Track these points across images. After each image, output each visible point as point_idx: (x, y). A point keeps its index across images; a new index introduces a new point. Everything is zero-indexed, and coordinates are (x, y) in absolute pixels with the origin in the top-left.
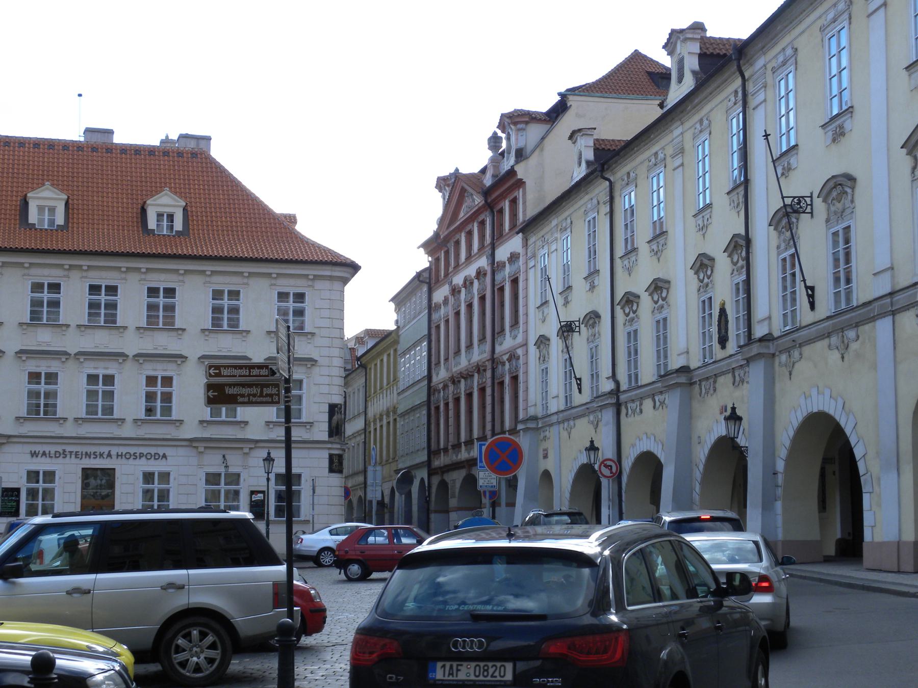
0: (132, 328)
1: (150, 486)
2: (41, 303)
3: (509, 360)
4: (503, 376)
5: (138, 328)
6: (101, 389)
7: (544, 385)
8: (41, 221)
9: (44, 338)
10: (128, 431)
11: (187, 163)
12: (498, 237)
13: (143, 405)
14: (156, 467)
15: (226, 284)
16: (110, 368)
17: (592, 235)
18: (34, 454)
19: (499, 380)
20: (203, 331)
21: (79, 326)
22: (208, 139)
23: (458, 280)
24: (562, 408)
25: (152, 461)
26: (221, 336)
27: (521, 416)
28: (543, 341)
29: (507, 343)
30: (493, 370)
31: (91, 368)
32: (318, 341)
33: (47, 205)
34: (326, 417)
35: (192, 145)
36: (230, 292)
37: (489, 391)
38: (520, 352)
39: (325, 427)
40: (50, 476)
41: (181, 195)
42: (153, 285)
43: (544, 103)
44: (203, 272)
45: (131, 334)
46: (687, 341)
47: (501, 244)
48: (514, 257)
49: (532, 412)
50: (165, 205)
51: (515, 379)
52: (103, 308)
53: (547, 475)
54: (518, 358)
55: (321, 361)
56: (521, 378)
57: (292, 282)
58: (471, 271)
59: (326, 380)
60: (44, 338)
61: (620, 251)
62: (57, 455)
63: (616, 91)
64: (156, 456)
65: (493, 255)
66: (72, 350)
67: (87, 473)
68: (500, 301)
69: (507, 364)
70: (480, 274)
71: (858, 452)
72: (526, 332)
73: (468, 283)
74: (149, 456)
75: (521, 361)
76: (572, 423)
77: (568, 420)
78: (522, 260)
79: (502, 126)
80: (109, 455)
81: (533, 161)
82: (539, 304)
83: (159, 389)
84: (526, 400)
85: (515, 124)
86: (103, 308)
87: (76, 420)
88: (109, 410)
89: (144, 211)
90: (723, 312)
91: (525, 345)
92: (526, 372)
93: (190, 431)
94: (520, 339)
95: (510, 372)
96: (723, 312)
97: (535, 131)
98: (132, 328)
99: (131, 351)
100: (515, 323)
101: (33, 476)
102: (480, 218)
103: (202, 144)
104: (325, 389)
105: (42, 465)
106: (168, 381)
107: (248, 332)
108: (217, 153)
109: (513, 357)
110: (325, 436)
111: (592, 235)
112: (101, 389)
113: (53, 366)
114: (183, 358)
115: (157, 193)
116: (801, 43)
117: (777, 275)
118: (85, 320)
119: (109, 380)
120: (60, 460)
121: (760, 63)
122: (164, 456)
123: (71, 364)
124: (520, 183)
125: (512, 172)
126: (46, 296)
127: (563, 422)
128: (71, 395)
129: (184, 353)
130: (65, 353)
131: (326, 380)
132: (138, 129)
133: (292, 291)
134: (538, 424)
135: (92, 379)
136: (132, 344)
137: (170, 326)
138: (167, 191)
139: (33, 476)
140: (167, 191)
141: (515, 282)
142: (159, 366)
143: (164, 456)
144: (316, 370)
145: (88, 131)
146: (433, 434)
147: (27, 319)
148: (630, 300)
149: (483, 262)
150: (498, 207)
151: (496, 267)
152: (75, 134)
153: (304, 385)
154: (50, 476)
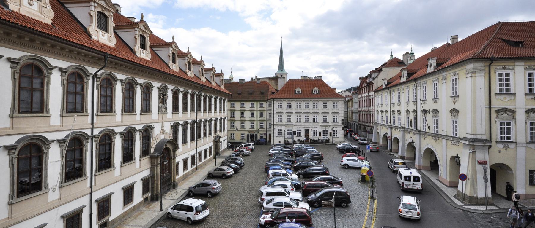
7: (378, 118)
9: (299, 111)
10: (311, 124)
12: (369, 91)
14: (315, 129)
16: (308, 115)
17: (386, 98)
19: (370, 115)
23: (363, 95)
29: (371, 109)
31: (305, 115)
40: (300, 130)
46: (404, 123)
48: (372, 95)
50: (316, 90)
53: (378, 132)
60: (299, 111)
61: (392, 102)
67: (306, 130)
68: (370, 102)
71: (438, 159)
81: (376, 79)
90: (411, 121)
93: (321, 124)
96: (411, 121)
97: (376, 74)
101: (298, 130)
105: (299, 129)
106: (326, 116)
111: (386, 98)
112: (307, 118)
113: (300, 115)
116: (428, 82)
117: (422, 121)
119: (308, 116)
121: (419, 81)
125: (372, 82)
128: (303, 119)
134: (377, 124)
135: (306, 116)
136: (311, 111)
139: (298, 130)
148: (393, 111)
149: (367, 94)
151: (369, 96)
154: (300, 130)
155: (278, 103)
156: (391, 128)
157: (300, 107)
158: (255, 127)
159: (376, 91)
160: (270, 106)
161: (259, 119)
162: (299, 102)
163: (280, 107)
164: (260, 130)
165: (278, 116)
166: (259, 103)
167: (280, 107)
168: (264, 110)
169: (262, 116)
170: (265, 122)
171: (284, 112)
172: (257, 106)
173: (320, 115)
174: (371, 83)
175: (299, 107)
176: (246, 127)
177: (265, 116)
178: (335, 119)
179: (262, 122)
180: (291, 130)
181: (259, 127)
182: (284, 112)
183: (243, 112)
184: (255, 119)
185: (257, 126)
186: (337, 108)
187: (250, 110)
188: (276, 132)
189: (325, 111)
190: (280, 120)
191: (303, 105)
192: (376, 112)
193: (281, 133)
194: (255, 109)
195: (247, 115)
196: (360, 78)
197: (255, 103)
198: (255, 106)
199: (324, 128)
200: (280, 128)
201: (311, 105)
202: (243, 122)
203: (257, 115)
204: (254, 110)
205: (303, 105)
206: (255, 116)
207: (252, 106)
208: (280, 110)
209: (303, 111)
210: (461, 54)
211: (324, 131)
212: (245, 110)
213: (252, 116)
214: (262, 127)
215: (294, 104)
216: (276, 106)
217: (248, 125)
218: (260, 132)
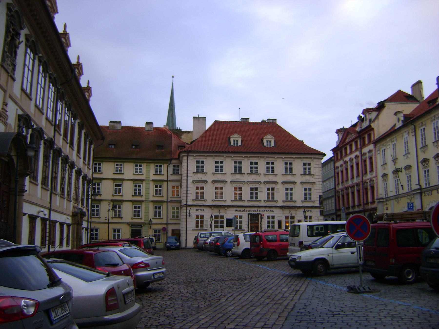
0: (262, 174)
1: (269, 220)
2: (218, 167)
3: (370, 182)
4: (367, 186)
5: (264, 174)
6: (254, 192)
8: (268, 145)
9: (238, 177)
11: (271, 126)
12: (364, 145)
13: (266, 196)
14: (271, 214)
15: (200, 159)
18: (236, 211)
19: (367, 188)
20: (282, 174)
21: (248, 174)
22: (276, 120)
24: (395, 194)
25: (270, 213)
26: (288, 176)
27: (376, 198)
28: (385, 176)
30: (363, 184)
32: (316, 177)
33: (236, 139)
34: (318, 199)
35: (271, 121)
36: (239, 162)
37: (361, 191)
38: (374, 179)
39: (318, 202)
41: (273, 135)
42: (252, 161)
43: (374, 105)
44: (282, 158)
45: (262, 176)
47: (364, 148)
48: (370, 151)
49: (380, 196)
51: (372, 187)
52: (254, 170)
54: (374, 181)
55: (317, 183)
56: (375, 187)
57: (307, 160)
58: (353, 156)
59: (318, 188)
60: (238, 177)
62: (243, 211)
63: (389, 101)
64: (271, 211)
65: (361, 151)
66: (246, 181)
68: (366, 164)
69: (369, 183)
70: (356, 157)
72: (376, 173)
73: (351, 160)
74: (268, 211)
75: (375, 182)
76: (399, 199)
77: (397, 198)
78: (373, 152)
79: (363, 113)
80: (257, 211)
81: (376, 122)
82: (382, 164)
83: (289, 192)
84: (377, 193)
85: (368, 112)
86: (254, 170)
87: (248, 201)
88: (256, 198)
89: (262, 141)
91: (376, 177)
92: (377, 185)
94: (374, 175)
95: (370, 185)
97: (374, 114)
98: (262, 174)
99: (262, 180)
100: (372, 170)
102: (356, 140)
103: (274, 121)
104: (318, 191)
106: (291, 189)
107: (207, 173)
108: (278, 123)
109: (371, 180)
110: (318, 205)
112: (254, 192)
114: (226, 182)
115: (266, 135)
118: (265, 172)
120: (244, 212)
122: (273, 211)
123: (246, 185)
124: (373, 129)
126: (200, 164)
127: (395, 199)
129: (207, 180)
130: (261, 182)
131: (318, 188)
132: (256, 117)
133: (307, 162)
135: (252, 189)
136: (262, 179)
137: (257, 173)
138: (236, 134)
140: (236, 134)
141: (371, 158)
142: (254, 185)
143: (273, 211)
144: (315, 185)
145: (242, 119)
146: (337, 203)
147: (303, 173)
150: (363, 136)
152: (239, 120)
153: (293, 190)
155: (198, 162)
156: (421, 194)
157: (240, 171)
158: (143, 214)
159: (376, 142)
160: (177, 171)
161: (151, 198)
162: (238, 160)
163: (200, 169)
164: (154, 221)
165: (197, 188)
166: (153, 167)
167: (200, 169)
168: (163, 181)
169: (158, 193)
170: (165, 205)
171: (210, 180)
172: (149, 171)
173: (280, 186)
174: (369, 129)
175: (238, 170)
176: (123, 214)
177: (164, 193)
178: (307, 193)
179: (157, 204)
180: (222, 217)
181: (151, 215)
182: (210, 180)
183: (118, 184)
184: (143, 199)
185: (147, 212)
186: (310, 174)
187: (133, 180)
188: (192, 224)
189: (289, 178)
190: (200, 196)
191: (246, 166)
192: (380, 178)
193: (202, 222)
194: (143, 177)
195: (128, 190)
196: (338, 132)
197: (144, 166)
198: (144, 171)
199: (287, 213)
200: (200, 213)
201: (262, 167)
202: (116, 205)
203: (148, 191)
204: (142, 180)
205: (246, 166)
206: (143, 192)
207: (138, 172)
208: (200, 176)
209: (246, 178)
210: (303, 259)
211: (287, 218)
212: (123, 180)
213: (137, 192)
214: (158, 215)
215: (229, 165)
216: (192, 166)
217: (127, 211)
218: (155, 227)
